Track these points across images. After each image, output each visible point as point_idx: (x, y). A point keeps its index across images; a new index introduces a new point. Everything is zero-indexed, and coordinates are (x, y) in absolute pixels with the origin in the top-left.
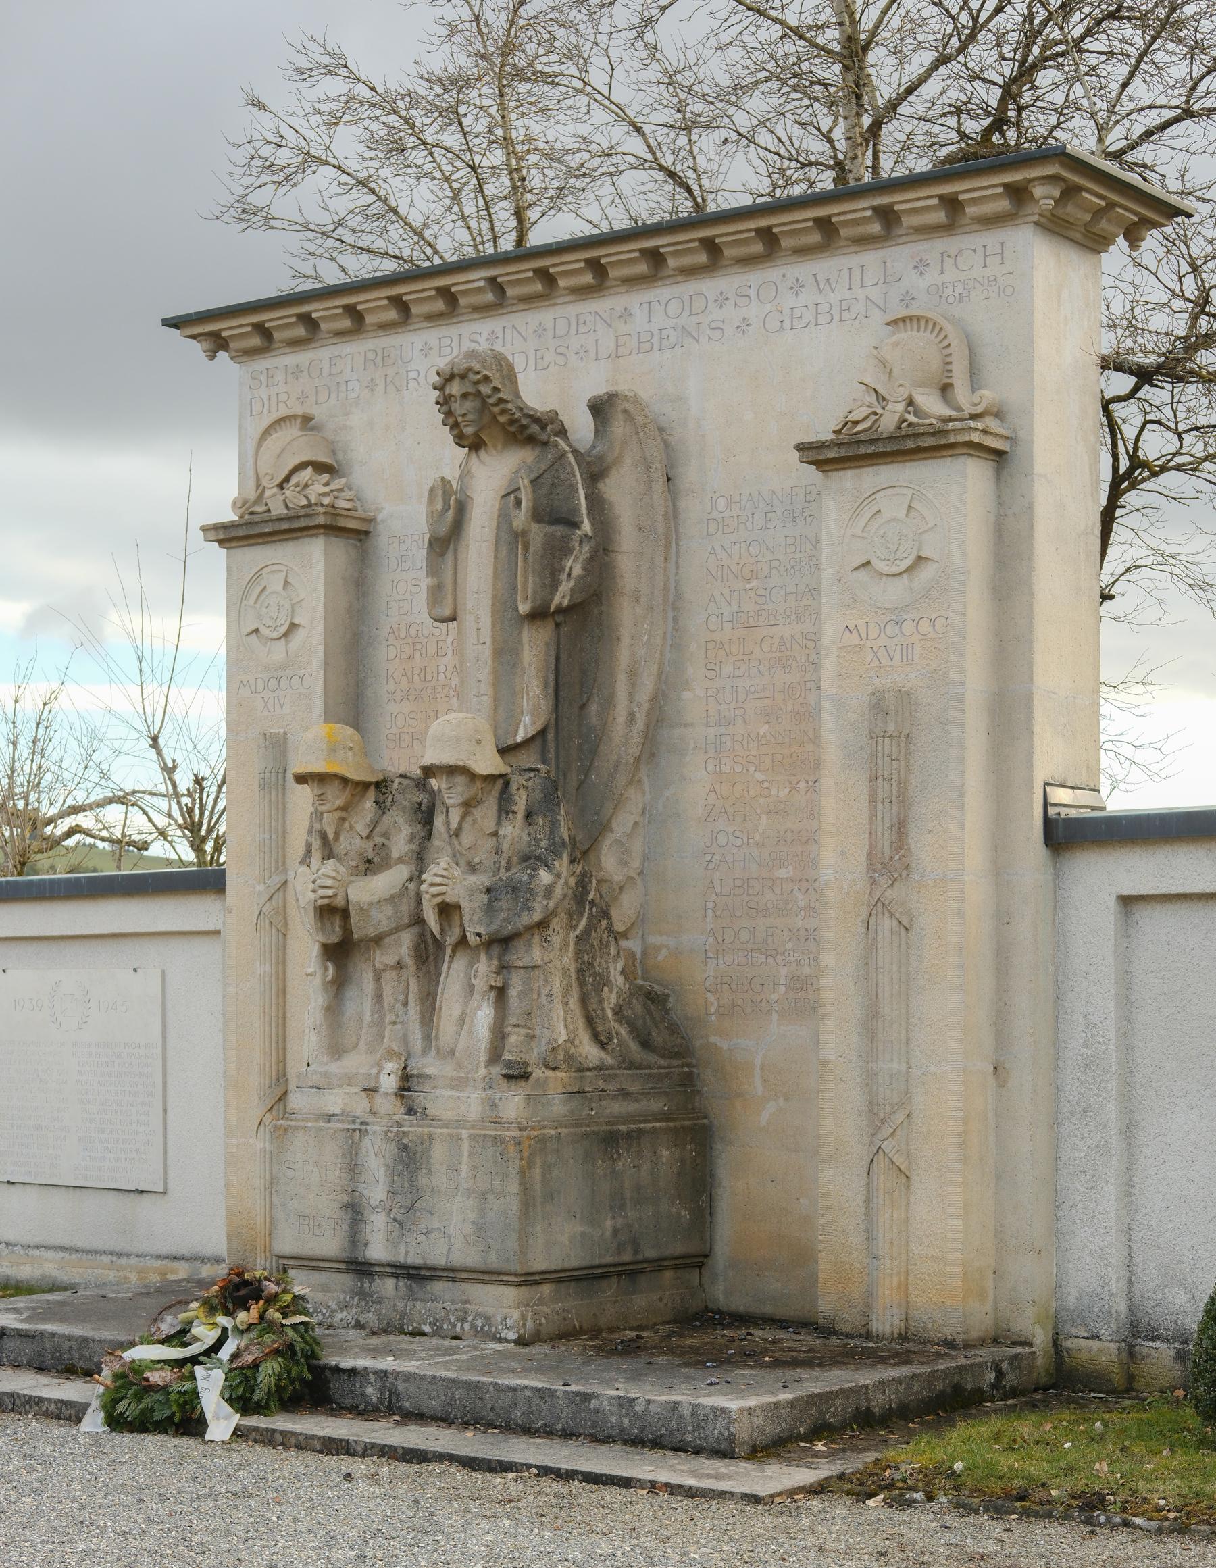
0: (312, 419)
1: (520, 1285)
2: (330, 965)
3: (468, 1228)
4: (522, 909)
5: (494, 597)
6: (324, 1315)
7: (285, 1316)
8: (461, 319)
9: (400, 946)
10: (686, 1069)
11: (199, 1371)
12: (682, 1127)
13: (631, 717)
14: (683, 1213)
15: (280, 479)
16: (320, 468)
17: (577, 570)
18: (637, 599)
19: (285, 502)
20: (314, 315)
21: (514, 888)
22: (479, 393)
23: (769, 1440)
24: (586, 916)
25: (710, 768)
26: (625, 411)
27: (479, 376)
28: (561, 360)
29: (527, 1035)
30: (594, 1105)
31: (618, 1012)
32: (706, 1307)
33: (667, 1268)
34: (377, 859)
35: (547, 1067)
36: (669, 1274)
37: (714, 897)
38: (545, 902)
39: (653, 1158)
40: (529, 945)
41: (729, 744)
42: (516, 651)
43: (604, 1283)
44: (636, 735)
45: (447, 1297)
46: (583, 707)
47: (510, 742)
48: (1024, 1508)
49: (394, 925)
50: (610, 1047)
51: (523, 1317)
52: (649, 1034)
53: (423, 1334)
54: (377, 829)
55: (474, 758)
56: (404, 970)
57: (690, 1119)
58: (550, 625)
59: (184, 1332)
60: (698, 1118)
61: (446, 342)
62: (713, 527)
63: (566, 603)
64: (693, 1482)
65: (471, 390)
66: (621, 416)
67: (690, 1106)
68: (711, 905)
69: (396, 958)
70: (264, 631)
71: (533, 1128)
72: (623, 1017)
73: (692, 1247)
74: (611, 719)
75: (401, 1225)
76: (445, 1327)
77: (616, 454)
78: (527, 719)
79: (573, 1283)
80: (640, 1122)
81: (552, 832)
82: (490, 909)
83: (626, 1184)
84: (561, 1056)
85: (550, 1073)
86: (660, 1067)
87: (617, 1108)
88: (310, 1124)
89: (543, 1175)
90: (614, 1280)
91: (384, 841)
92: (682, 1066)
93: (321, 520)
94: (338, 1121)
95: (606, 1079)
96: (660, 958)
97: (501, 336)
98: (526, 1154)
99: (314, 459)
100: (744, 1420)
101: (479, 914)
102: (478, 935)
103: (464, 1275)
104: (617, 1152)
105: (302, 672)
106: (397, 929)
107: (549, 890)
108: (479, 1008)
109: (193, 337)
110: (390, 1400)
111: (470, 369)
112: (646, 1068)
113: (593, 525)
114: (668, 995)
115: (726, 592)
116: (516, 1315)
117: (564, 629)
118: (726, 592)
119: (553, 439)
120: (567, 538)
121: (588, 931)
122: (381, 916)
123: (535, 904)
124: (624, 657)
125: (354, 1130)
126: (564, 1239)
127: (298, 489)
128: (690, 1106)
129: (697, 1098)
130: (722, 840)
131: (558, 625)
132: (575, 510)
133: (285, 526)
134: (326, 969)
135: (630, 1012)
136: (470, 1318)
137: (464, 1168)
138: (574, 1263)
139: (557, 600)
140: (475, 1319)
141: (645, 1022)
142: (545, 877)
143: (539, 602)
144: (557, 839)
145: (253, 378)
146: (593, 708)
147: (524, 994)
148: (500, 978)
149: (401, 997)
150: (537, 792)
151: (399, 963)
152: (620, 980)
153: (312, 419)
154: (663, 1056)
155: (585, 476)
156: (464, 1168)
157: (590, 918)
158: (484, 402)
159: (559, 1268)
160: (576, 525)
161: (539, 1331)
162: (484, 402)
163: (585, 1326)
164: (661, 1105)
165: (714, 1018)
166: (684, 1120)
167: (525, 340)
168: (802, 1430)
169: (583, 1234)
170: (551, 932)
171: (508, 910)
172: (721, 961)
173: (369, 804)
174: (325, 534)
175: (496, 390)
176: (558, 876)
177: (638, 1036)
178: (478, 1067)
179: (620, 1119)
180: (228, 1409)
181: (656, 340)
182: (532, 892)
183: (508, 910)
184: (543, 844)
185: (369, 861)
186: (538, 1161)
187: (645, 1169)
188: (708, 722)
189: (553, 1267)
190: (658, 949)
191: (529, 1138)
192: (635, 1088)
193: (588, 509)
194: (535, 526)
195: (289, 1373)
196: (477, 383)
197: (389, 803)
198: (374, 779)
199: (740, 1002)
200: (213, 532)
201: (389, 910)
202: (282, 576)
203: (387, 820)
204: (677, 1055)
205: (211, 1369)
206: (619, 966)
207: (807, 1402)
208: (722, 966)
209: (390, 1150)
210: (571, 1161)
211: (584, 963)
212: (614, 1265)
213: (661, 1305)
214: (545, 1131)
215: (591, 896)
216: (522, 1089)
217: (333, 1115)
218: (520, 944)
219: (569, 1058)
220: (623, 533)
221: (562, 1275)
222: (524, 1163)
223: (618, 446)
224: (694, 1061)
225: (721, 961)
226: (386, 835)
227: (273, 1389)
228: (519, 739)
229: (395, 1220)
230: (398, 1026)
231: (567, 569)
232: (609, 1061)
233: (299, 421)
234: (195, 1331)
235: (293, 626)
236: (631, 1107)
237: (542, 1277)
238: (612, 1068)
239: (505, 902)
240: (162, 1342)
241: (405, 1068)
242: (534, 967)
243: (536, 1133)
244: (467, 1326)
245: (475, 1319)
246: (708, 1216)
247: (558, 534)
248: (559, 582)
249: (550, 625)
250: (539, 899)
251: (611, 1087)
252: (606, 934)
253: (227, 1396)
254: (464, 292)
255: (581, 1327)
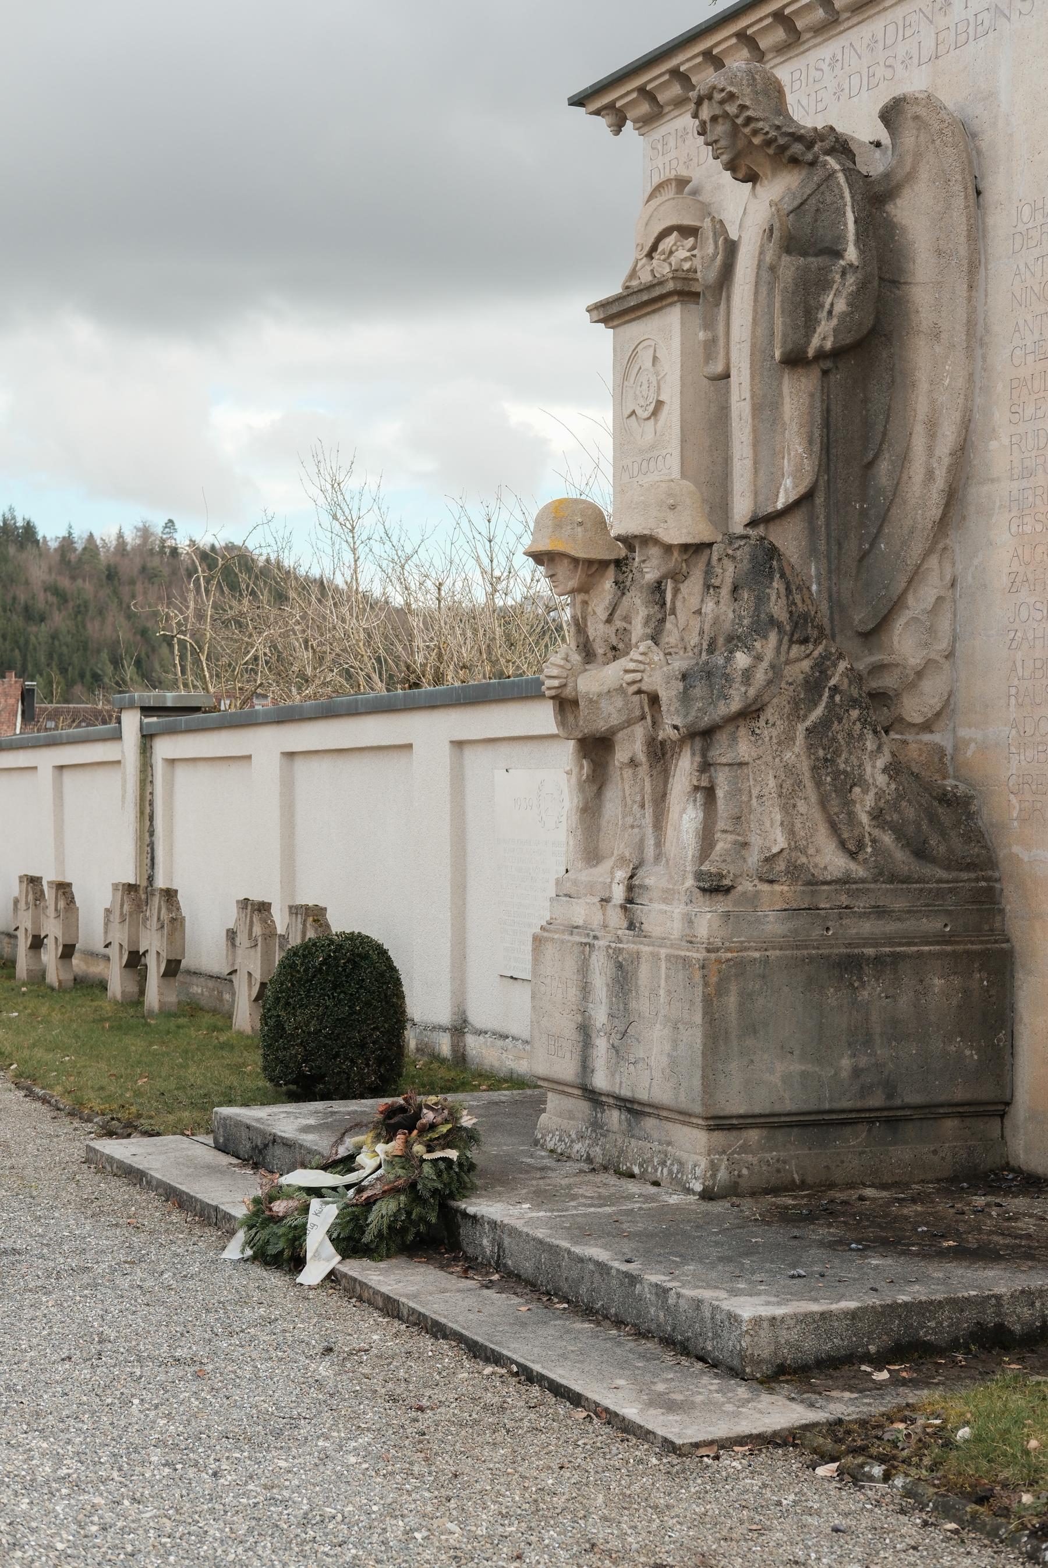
0: (688, 182)
1: (710, 1129)
2: (585, 762)
3: (665, 1060)
4: (718, 698)
5: (753, 345)
6: (566, 1144)
7: (430, 1149)
8: (806, 46)
9: (634, 742)
10: (984, 884)
11: (315, 1203)
12: (967, 952)
13: (930, 475)
14: (967, 1052)
15: (647, 249)
16: (688, 231)
17: (841, 306)
18: (937, 336)
19: (652, 271)
20: (682, 69)
21: (708, 674)
22: (726, 115)
23: (811, 1359)
24: (823, 704)
25: (1014, 529)
26: (916, 118)
27: (723, 94)
28: (888, 74)
29: (735, 842)
30: (830, 924)
31: (877, 815)
32: (1008, 1163)
33: (946, 1116)
34: (621, 646)
35: (761, 879)
36: (950, 1124)
37: (1016, 682)
38: (743, 689)
39: (919, 987)
40: (734, 739)
41: (1031, 499)
42: (775, 405)
43: (848, 1131)
44: (935, 496)
45: (655, 1136)
46: (870, 465)
47: (770, 510)
48: (974, 1515)
49: (624, 718)
50: (861, 857)
51: (714, 1167)
52: (925, 842)
53: (632, 1176)
54: (618, 613)
55: (665, 526)
56: (640, 768)
57: (982, 942)
58: (815, 373)
59: (351, 1158)
60: (996, 942)
61: (797, 75)
62: (1018, 239)
63: (828, 345)
64: (631, 1412)
65: (718, 111)
66: (910, 123)
67: (986, 927)
68: (1013, 691)
69: (630, 755)
70: (639, 412)
71: (729, 950)
72: (886, 822)
73: (986, 1092)
74: (905, 477)
75: (617, 1052)
76: (650, 1170)
77: (908, 169)
78: (788, 482)
79: (795, 1130)
80: (901, 945)
81: (757, 608)
82: (685, 697)
83: (874, 1017)
84: (781, 866)
85: (765, 887)
86: (940, 881)
87: (868, 927)
88: (556, 936)
89: (741, 1004)
90: (863, 1128)
91: (625, 625)
92: (977, 880)
93: (670, 286)
94: (578, 934)
95: (850, 893)
96: (969, 753)
97: (840, 58)
98: (714, 980)
99: (679, 222)
100: (762, 1333)
101: (676, 704)
102: (675, 727)
103: (665, 1114)
104: (860, 979)
105: (664, 453)
106: (629, 723)
107: (747, 675)
108: (684, 810)
109: (597, 113)
110: (499, 1256)
111: (714, 88)
112: (916, 882)
113: (861, 252)
114: (972, 797)
115: (1029, 317)
116: (703, 1163)
117: (836, 377)
118: (1029, 317)
119: (822, 158)
120: (825, 270)
121: (825, 723)
122: (611, 709)
123: (732, 691)
124: (921, 406)
125: (585, 944)
126: (775, 1079)
127: (663, 257)
128: (986, 927)
129: (998, 918)
130: (1024, 614)
131: (825, 373)
132: (841, 238)
133: (645, 297)
134: (582, 767)
135: (895, 816)
136: (669, 1162)
137: (662, 992)
138: (789, 1106)
139: (815, 342)
140: (672, 1164)
141: (919, 826)
142: (742, 660)
143: (790, 346)
144: (763, 616)
145: (653, 149)
146: (884, 466)
147: (735, 792)
148: (705, 777)
149: (638, 798)
150: (745, 562)
151: (632, 760)
152: (882, 779)
153: (688, 182)
154: (948, 868)
155: (859, 197)
156: (662, 992)
157: (831, 706)
158: (734, 124)
159: (767, 1112)
160: (838, 254)
161: (736, 1184)
162: (734, 124)
163: (810, 1180)
164: (939, 925)
165: (1016, 824)
166: (972, 943)
167: (860, 58)
168: (872, 1349)
169: (803, 1074)
170: (762, 723)
171: (702, 698)
172: (1022, 758)
173: (608, 584)
174: (682, 302)
175: (743, 108)
176: (759, 658)
177: (908, 844)
178: (684, 876)
179: (867, 942)
180: (330, 1249)
181: (971, 30)
182: (727, 677)
183: (702, 698)
184: (746, 622)
185: (614, 648)
186: (734, 988)
187: (904, 1001)
188: (1012, 475)
189: (757, 1110)
190: (967, 743)
191: (719, 961)
192: (899, 904)
193: (857, 234)
194: (786, 259)
195: (409, 1214)
196: (722, 102)
197: (628, 584)
198: (613, 557)
199: (1038, 805)
200: (601, 310)
201: (619, 702)
202: (651, 351)
203: (626, 601)
204: (971, 867)
205: (327, 1203)
206: (880, 763)
207: (882, 1314)
208: (1023, 763)
209: (610, 969)
210: (786, 989)
211: (818, 759)
212: (851, 1111)
213: (936, 1158)
214: (745, 954)
215: (833, 682)
216: (723, 904)
217: (577, 927)
218: (722, 738)
219: (794, 871)
220: (918, 261)
221: (776, 1120)
222: (711, 990)
223: (909, 160)
224: (997, 875)
225: (1022, 758)
226: (627, 619)
227: (385, 1231)
228: (780, 505)
229: (613, 1046)
230: (636, 830)
231: (827, 306)
232: (859, 871)
233: (674, 184)
234: (359, 1159)
235: (660, 404)
236: (890, 927)
237: (741, 1121)
238: (863, 881)
239: (699, 691)
240: (325, 1168)
241: (631, 877)
242: (741, 764)
243: (729, 955)
244: (665, 1171)
245: (672, 1164)
246: (1007, 1057)
247: (815, 265)
248: (818, 322)
249: (815, 373)
250: (737, 685)
251: (861, 904)
252: (858, 725)
253: (335, 1236)
254: (796, 12)
255: (803, 1182)
